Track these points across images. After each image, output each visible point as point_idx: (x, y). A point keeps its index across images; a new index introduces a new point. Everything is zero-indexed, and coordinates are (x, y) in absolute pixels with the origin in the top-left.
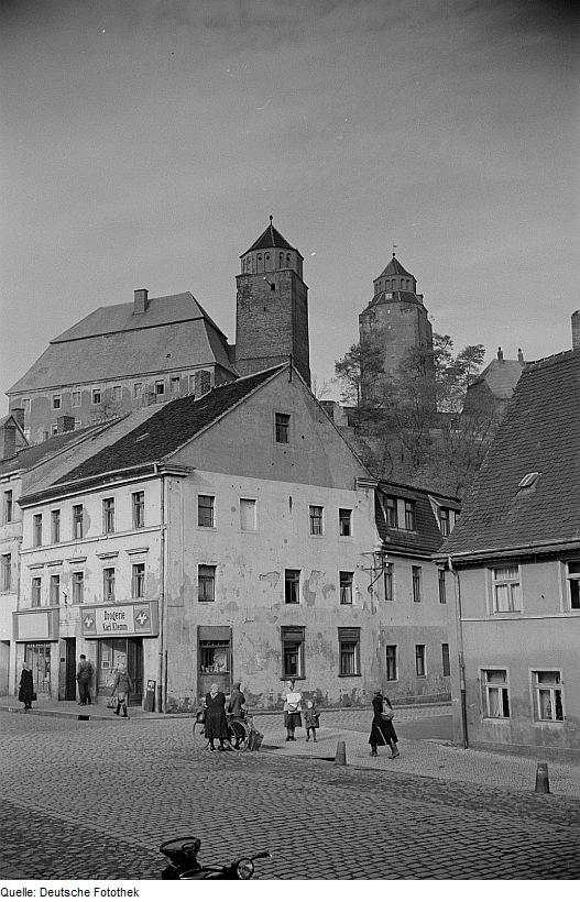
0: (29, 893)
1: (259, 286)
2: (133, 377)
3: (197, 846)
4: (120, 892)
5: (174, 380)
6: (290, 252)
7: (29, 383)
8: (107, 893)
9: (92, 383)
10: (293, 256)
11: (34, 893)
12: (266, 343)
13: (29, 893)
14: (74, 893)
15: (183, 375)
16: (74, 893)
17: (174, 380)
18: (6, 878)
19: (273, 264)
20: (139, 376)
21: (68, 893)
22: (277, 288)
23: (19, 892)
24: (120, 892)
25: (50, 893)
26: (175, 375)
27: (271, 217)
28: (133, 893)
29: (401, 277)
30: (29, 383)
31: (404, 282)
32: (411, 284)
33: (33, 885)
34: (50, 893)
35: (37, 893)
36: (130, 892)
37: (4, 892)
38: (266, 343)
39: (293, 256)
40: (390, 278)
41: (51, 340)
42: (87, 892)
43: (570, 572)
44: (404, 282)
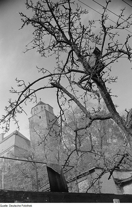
0: (7, 206)
4: (28, 206)
8: (25, 206)
13: (7, 206)
14: (17, 206)
16: (17, 206)
19: (40, 109)
23: (4, 206)
24: (28, 206)
25: (12, 206)
28: (31, 206)
34: (12, 206)
35: (9, 206)
36: (30, 206)
37: (1, 206)
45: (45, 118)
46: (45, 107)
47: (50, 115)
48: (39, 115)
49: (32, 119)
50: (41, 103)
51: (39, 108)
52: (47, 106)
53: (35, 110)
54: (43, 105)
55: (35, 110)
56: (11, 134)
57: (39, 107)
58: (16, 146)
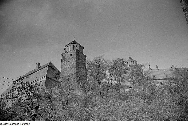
0: (6, 124)
1: (67, 55)
3: (51, 66)
4: (26, 124)
6: (134, 61)
8: (23, 124)
12: (69, 71)
13: (6, 124)
14: (16, 124)
16: (16, 124)
19: (71, 48)
23: (4, 124)
24: (26, 124)
25: (11, 124)
28: (28, 124)
29: (132, 61)
31: (133, 62)
32: (135, 63)
34: (11, 124)
35: (8, 124)
36: (28, 124)
37: (1, 124)
38: (69, 71)
40: (128, 62)
44: (133, 62)
45: (75, 56)
46: (77, 46)
47: (80, 53)
48: (71, 53)
49: (64, 55)
50: (74, 42)
51: (71, 46)
52: (78, 46)
53: (68, 48)
54: (76, 45)
55: (68, 48)
56: (45, 65)
57: (72, 45)
58: (47, 77)
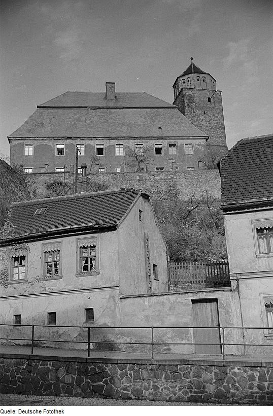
0: (13, 412)
2: (135, 138)
4: (55, 411)
5: (170, 145)
7: (29, 131)
8: (49, 412)
9: (96, 138)
10: (208, 78)
11: (16, 412)
13: (13, 412)
14: (34, 412)
15: (179, 142)
16: (34, 412)
17: (170, 145)
18: (3, 404)
20: (141, 138)
21: (31, 412)
22: (212, 100)
23: (9, 411)
24: (55, 411)
25: (23, 412)
26: (172, 142)
27: (192, 59)
28: (61, 412)
30: (29, 131)
33: (15, 408)
34: (23, 412)
35: (17, 412)
36: (60, 411)
37: (2, 411)
39: (208, 78)
41: (39, 105)
42: (40, 411)
43: (156, 148)
